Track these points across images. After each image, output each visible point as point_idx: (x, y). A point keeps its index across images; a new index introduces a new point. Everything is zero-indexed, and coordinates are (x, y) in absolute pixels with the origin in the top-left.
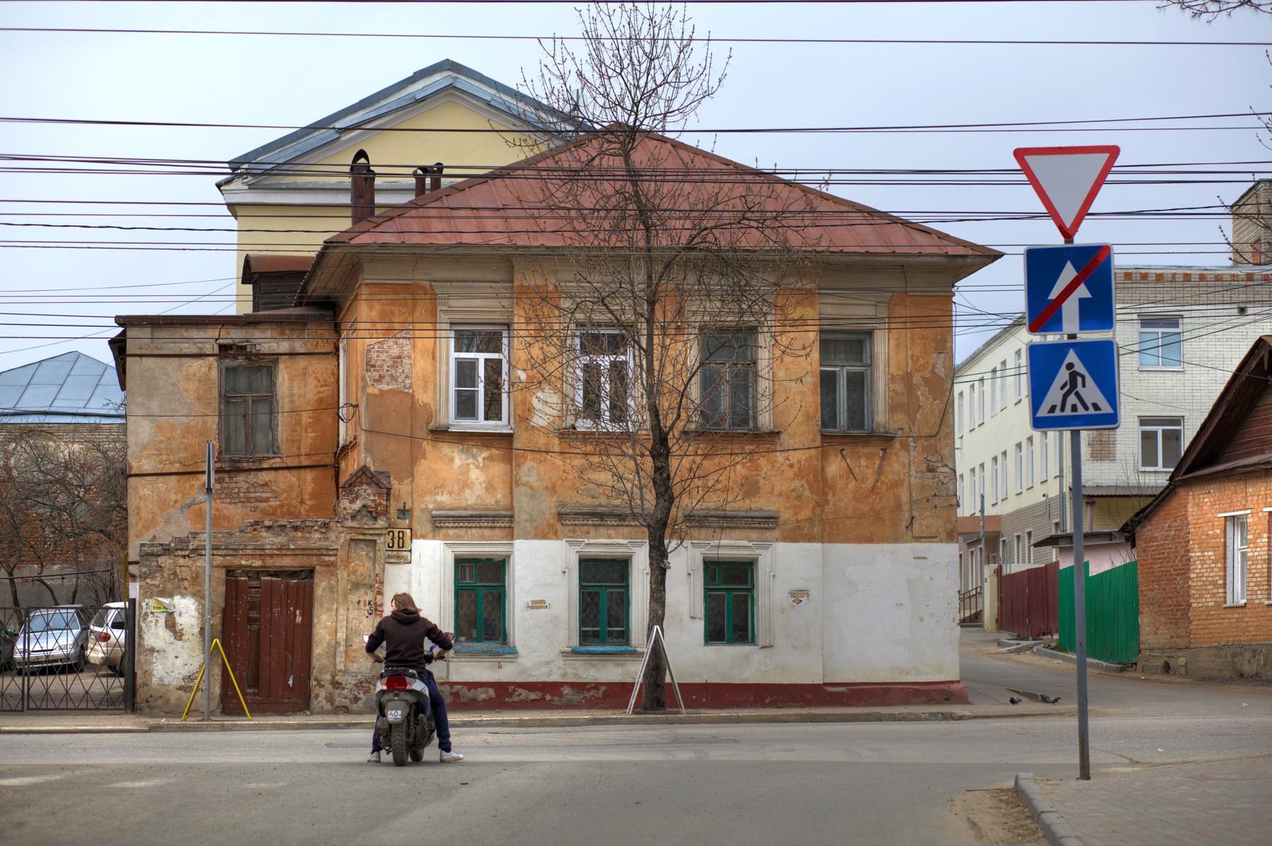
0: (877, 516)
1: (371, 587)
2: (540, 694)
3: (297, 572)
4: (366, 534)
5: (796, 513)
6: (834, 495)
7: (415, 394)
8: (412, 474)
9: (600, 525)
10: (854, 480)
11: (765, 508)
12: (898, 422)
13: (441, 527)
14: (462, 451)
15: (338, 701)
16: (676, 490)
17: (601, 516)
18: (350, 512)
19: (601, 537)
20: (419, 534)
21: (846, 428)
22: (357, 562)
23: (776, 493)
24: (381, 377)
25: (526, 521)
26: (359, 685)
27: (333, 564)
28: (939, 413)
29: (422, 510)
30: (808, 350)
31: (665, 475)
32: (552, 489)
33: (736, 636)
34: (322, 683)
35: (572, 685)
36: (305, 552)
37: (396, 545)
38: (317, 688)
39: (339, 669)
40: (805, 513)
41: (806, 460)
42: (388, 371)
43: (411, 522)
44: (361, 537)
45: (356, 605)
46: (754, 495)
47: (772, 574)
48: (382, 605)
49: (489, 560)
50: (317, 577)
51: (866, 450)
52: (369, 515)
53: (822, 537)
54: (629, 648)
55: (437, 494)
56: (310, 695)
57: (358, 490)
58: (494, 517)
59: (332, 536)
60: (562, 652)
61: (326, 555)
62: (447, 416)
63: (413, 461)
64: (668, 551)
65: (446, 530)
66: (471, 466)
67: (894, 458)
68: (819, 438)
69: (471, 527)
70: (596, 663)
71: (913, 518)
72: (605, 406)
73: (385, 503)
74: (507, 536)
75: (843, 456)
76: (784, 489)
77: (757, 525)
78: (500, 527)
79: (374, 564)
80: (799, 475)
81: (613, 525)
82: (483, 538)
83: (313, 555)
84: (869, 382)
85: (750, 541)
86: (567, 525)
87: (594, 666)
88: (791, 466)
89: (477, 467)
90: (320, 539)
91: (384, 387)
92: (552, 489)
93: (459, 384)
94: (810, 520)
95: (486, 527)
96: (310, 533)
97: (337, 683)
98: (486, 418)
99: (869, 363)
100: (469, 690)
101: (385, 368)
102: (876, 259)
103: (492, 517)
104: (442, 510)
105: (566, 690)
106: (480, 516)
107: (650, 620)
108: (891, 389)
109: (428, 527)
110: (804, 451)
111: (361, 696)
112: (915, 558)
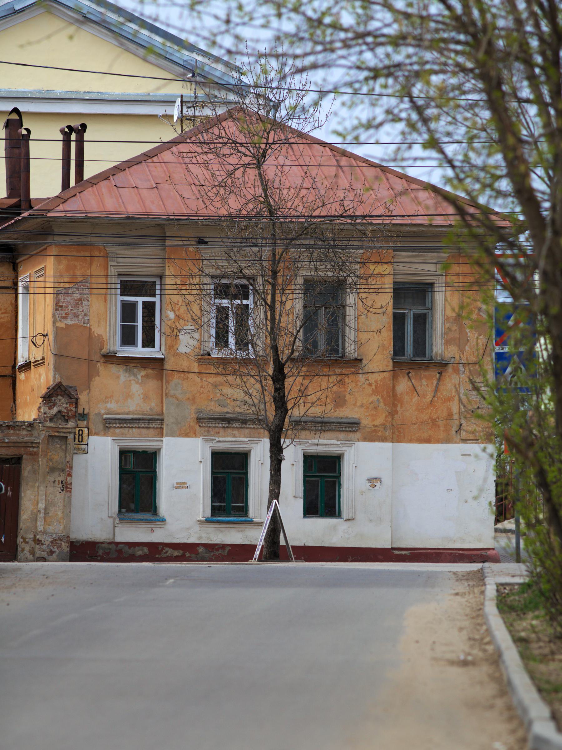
0: (434, 422)
1: (63, 470)
2: (181, 552)
3: (8, 459)
4: (60, 432)
5: (373, 420)
6: (401, 407)
7: (92, 327)
8: (89, 387)
9: (227, 427)
10: (417, 396)
11: (350, 416)
12: (452, 352)
13: (110, 427)
14: (126, 371)
15: (38, 554)
16: (289, 406)
17: (229, 420)
18: (49, 415)
19: (228, 436)
20: (94, 431)
21: (411, 356)
22: (53, 452)
23: (358, 404)
24: (67, 315)
25: (173, 423)
26: (54, 542)
27: (36, 454)
28: (483, 345)
29: (96, 414)
30: (384, 309)
31: (282, 394)
32: (193, 400)
33: (326, 511)
34: (27, 540)
35: (205, 546)
36: (16, 444)
37: (77, 440)
38: (23, 544)
39: (39, 530)
40: (379, 421)
41: (381, 381)
42: (72, 310)
43: (88, 423)
44: (57, 434)
45: (52, 484)
46: (342, 406)
47: (354, 465)
48: (71, 484)
49: (145, 452)
50: (24, 464)
51: (427, 373)
52: (62, 418)
53: (392, 438)
54: (248, 519)
55: (108, 402)
56: (17, 549)
57: (55, 400)
58: (150, 420)
59: (35, 433)
60: (198, 521)
61: (30, 447)
62: (115, 345)
63: (90, 378)
64: (283, 447)
65: (114, 429)
66: (132, 382)
67: (448, 379)
68: (391, 363)
69: (132, 427)
70: (223, 529)
71: (461, 425)
72: (232, 340)
73: (74, 409)
74: (158, 435)
75: (409, 377)
76: (365, 402)
77: (344, 429)
78: (154, 428)
79: (65, 454)
80: (376, 391)
81: (237, 428)
82: (140, 435)
83: (21, 447)
84: (430, 321)
85: (338, 440)
86: (203, 427)
87: (222, 532)
88: (370, 385)
89: (137, 383)
90: (26, 435)
91: (69, 322)
92: (193, 400)
93: (123, 320)
94: (384, 426)
95: (143, 428)
96: (19, 430)
97: (38, 540)
98: (143, 346)
99: (430, 307)
100: (130, 548)
101: (70, 308)
102: (437, 229)
103: (147, 420)
104: (111, 414)
105: (201, 550)
106: (139, 419)
107: (270, 496)
108: (447, 327)
109: (101, 427)
110: (380, 374)
111: (55, 550)
112: (462, 455)
